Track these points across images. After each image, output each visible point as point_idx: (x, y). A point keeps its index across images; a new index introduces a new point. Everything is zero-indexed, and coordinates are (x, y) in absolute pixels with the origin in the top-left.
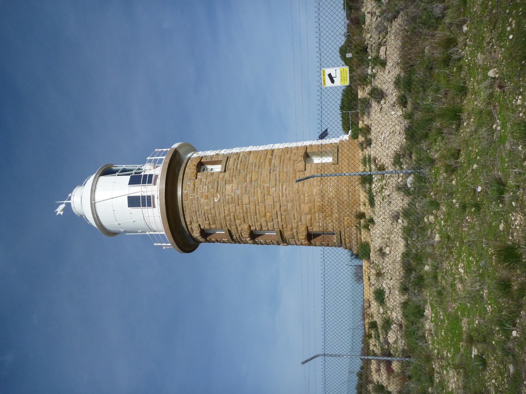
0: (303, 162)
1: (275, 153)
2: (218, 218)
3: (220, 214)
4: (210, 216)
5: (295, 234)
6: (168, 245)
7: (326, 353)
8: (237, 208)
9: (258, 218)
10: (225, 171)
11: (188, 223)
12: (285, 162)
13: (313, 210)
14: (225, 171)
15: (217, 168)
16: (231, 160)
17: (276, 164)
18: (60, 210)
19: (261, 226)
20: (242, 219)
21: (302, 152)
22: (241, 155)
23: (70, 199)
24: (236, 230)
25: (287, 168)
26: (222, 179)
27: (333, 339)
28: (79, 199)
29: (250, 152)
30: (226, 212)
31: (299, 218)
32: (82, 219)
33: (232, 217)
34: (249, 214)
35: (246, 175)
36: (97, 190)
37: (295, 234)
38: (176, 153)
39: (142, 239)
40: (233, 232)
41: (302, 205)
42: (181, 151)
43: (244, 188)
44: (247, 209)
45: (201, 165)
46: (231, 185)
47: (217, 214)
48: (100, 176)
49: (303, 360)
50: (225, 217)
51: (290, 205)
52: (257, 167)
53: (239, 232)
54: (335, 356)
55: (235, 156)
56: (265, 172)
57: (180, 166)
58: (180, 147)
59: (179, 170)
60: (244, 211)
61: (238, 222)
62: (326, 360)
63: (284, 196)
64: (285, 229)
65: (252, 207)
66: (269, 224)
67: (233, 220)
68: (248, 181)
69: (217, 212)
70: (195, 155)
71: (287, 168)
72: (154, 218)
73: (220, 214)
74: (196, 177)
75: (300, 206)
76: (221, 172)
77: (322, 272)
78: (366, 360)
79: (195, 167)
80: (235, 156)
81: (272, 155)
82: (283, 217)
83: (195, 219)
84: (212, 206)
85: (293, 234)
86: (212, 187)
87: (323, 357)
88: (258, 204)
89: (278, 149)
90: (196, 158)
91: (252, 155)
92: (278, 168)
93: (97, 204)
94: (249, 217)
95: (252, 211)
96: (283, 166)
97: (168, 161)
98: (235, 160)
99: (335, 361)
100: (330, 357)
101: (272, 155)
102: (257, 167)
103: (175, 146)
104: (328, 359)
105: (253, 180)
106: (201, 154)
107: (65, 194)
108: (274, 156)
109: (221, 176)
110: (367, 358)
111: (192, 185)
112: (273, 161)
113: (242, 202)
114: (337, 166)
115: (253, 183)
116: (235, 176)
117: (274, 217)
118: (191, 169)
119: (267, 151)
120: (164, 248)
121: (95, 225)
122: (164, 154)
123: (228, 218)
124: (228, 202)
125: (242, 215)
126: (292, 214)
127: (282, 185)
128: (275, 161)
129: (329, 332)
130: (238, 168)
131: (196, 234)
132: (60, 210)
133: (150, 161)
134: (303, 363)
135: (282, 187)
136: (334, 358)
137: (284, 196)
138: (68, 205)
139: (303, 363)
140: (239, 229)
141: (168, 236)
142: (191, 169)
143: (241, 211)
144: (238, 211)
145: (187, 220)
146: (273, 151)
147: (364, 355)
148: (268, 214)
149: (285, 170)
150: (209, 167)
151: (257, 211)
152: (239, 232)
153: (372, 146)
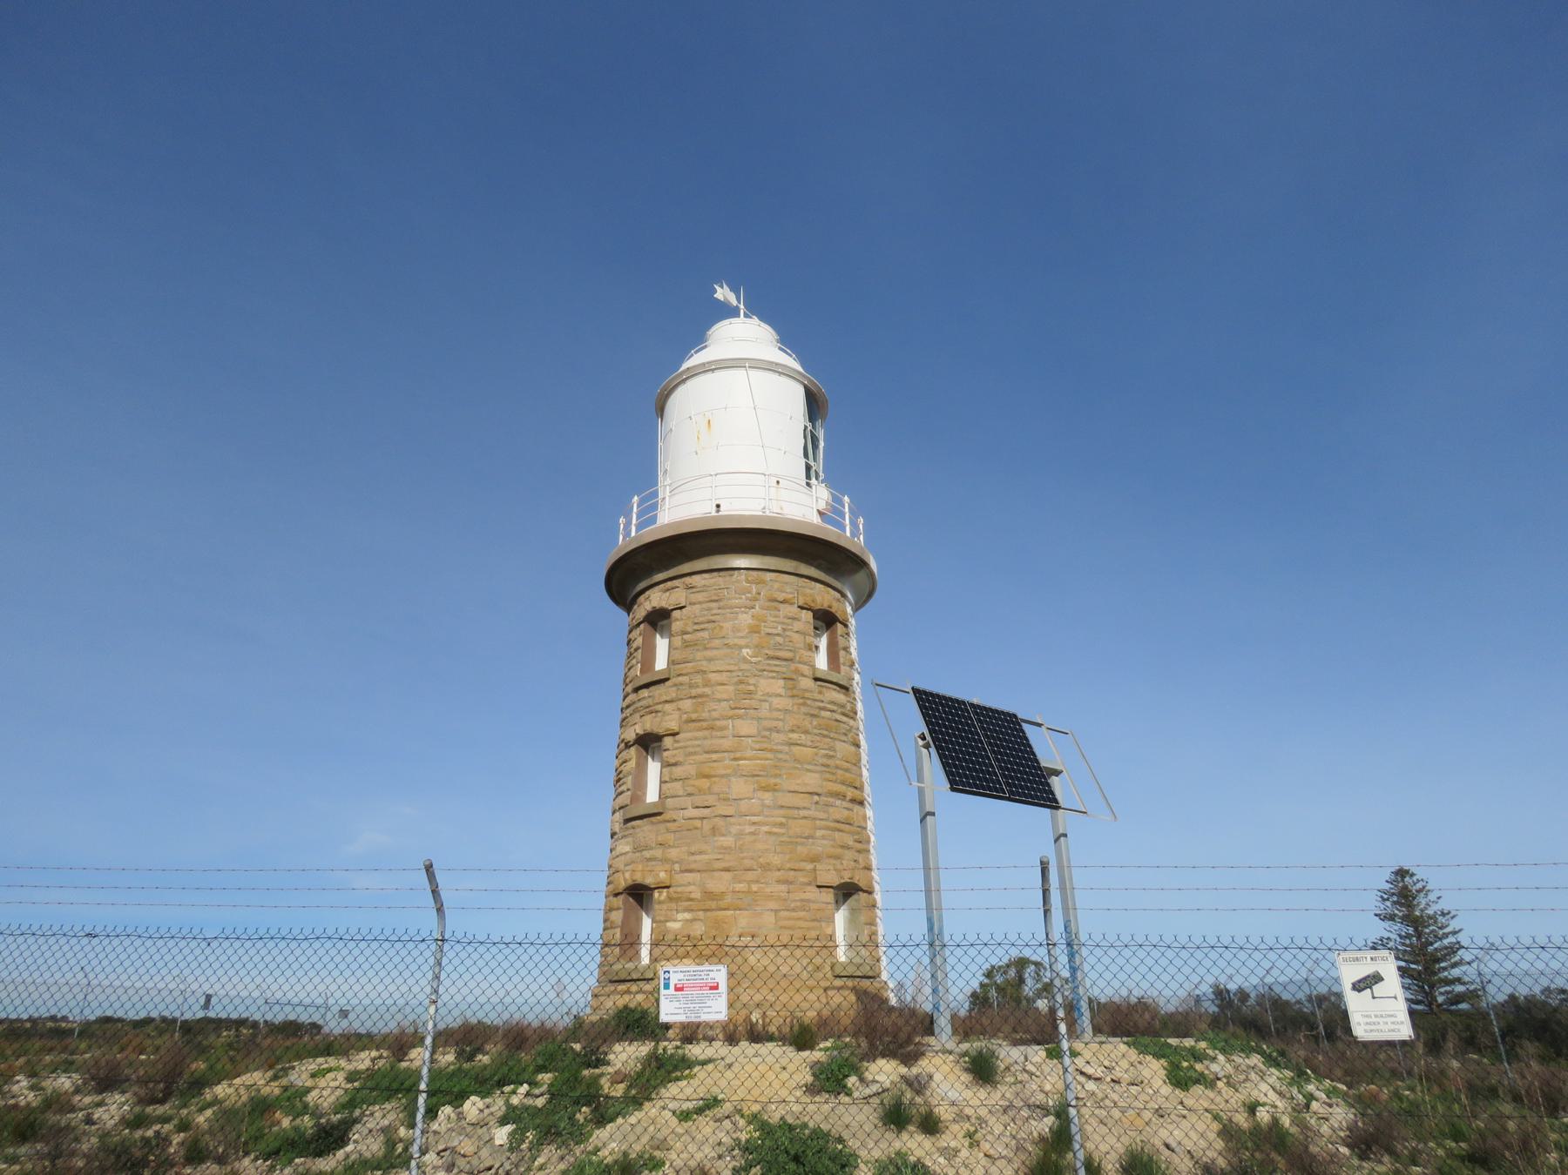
0: (836, 882)
1: (857, 808)
2: (699, 655)
3: (710, 660)
4: (705, 634)
5: (647, 854)
6: (630, 533)
7: (446, 947)
8: (724, 704)
9: (697, 758)
10: (816, 679)
11: (688, 580)
12: (837, 834)
13: (713, 905)
14: (816, 679)
15: (821, 662)
16: (840, 697)
17: (831, 810)
18: (723, 293)
19: (675, 764)
20: (694, 716)
21: (859, 879)
22: (852, 722)
23: (746, 316)
24: (665, 698)
25: (823, 837)
26: (797, 671)
27: (542, 965)
28: (742, 336)
29: (858, 746)
30: (712, 676)
31: (693, 866)
32: (697, 339)
33: (699, 691)
34: (706, 733)
35: (806, 732)
36: (775, 377)
37: (647, 854)
38: (858, 563)
39: (641, 470)
40: (658, 692)
41: (727, 876)
42: (860, 576)
43: (775, 723)
44: (722, 729)
45: (826, 620)
46: (782, 692)
47: (709, 653)
48: (806, 387)
49: (1445, 893)
50: (704, 672)
51: (727, 841)
52: (825, 761)
53: (659, 707)
54: (437, 977)
55: (849, 706)
56: (812, 780)
57: (828, 571)
58: (871, 574)
59: (818, 567)
60: (718, 723)
61: (687, 704)
62: (422, 946)
63: (752, 829)
64: (662, 827)
65: (727, 743)
66: (678, 785)
67: (694, 692)
68: (792, 735)
69: (715, 652)
70: (849, 610)
71: (823, 837)
72: (683, 504)
73: (710, 660)
74: (802, 608)
75: (727, 870)
76: (813, 667)
77: (1183, 940)
78: (416, 1084)
79: (825, 606)
80: (849, 706)
81: (853, 801)
82: (698, 823)
83: (700, 597)
84: (730, 642)
85: (647, 848)
86: (778, 647)
87: (1042, 937)
88: (735, 759)
89: (865, 818)
90: (845, 613)
91: (853, 749)
92: (822, 815)
93: (742, 371)
94: (700, 734)
95: (715, 741)
96: (827, 828)
97: (842, 543)
98: (843, 706)
99: (418, 975)
100: (432, 961)
101: (853, 801)
102: (825, 761)
103: (873, 565)
104: (428, 953)
105: (796, 749)
106: (852, 622)
107: (757, 309)
108: (850, 805)
109: (805, 669)
110: (423, 1086)
111: (781, 597)
112: (838, 802)
113: (739, 717)
114: (829, 975)
115: (786, 748)
116: (804, 704)
117: (699, 800)
118: (823, 596)
119: (860, 788)
120: (622, 520)
121: (685, 366)
122: (855, 533)
123: (698, 679)
124: (741, 682)
125: (705, 715)
126: (704, 847)
127: (782, 825)
128: (840, 810)
129: (537, 958)
130: (824, 714)
131: (655, 599)
132: (723, 293)
133: (837, 500)
134: (429, 869)
135: (775, 825)
136: (430, 975)
137: (752, 829)
138: (732, 312)
139: (429, 869)
140: (668, 707)
141: (651, 534)
142: (823, 596)
143: (715, 714)
144: (713, 705)
145: (696, 578)
146: (861, 803)
147: (432, 1079)
148: (704, 783)
149: (819, 833)
150: (823, 642)
151: (714, 756)
152: (659, 707)
153: (321, 1022)
